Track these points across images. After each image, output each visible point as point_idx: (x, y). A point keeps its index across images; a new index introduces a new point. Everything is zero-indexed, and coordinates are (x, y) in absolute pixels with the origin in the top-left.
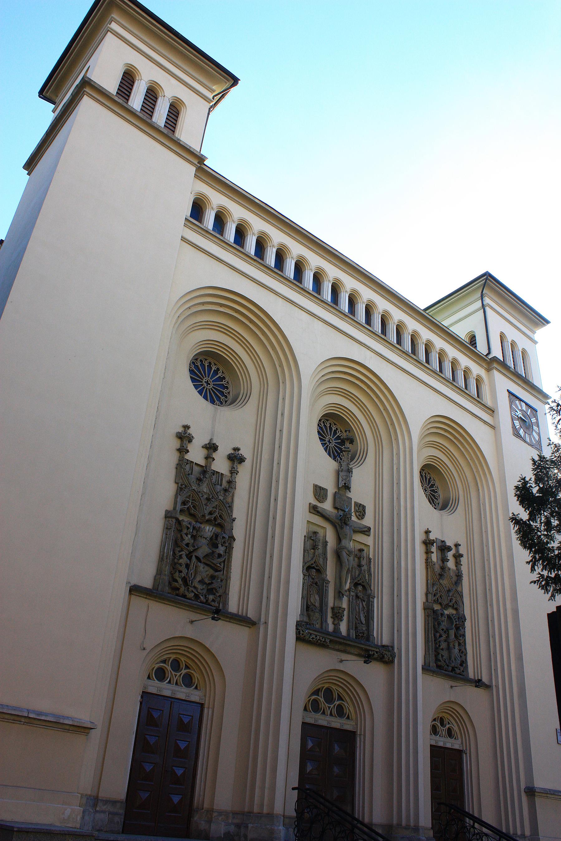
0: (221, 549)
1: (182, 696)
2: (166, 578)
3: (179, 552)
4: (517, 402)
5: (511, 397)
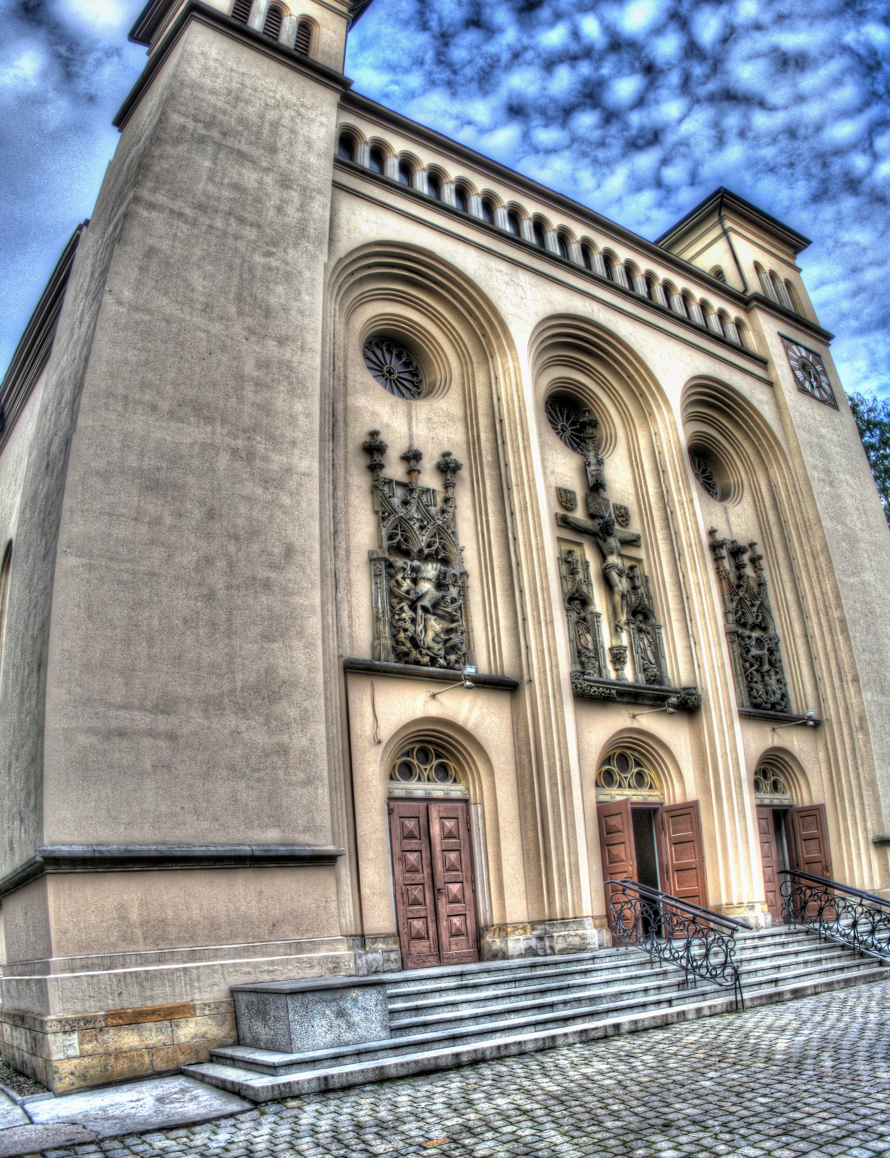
0: (453, 592)
1: (439, 794)
2: (388, 642)
3: (399, 603)
4: (794, 347)
5: (785, 341)
